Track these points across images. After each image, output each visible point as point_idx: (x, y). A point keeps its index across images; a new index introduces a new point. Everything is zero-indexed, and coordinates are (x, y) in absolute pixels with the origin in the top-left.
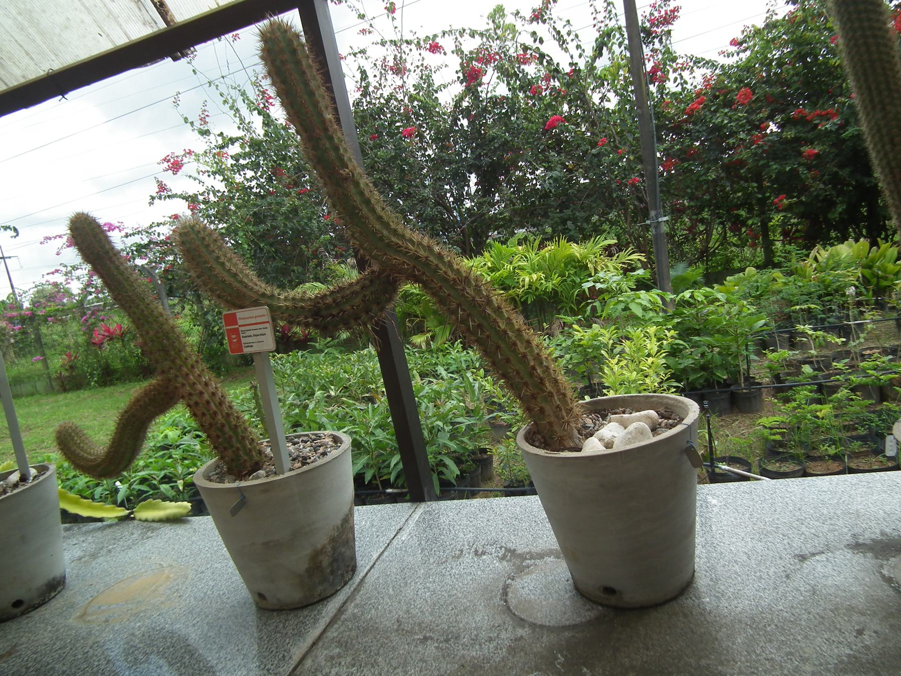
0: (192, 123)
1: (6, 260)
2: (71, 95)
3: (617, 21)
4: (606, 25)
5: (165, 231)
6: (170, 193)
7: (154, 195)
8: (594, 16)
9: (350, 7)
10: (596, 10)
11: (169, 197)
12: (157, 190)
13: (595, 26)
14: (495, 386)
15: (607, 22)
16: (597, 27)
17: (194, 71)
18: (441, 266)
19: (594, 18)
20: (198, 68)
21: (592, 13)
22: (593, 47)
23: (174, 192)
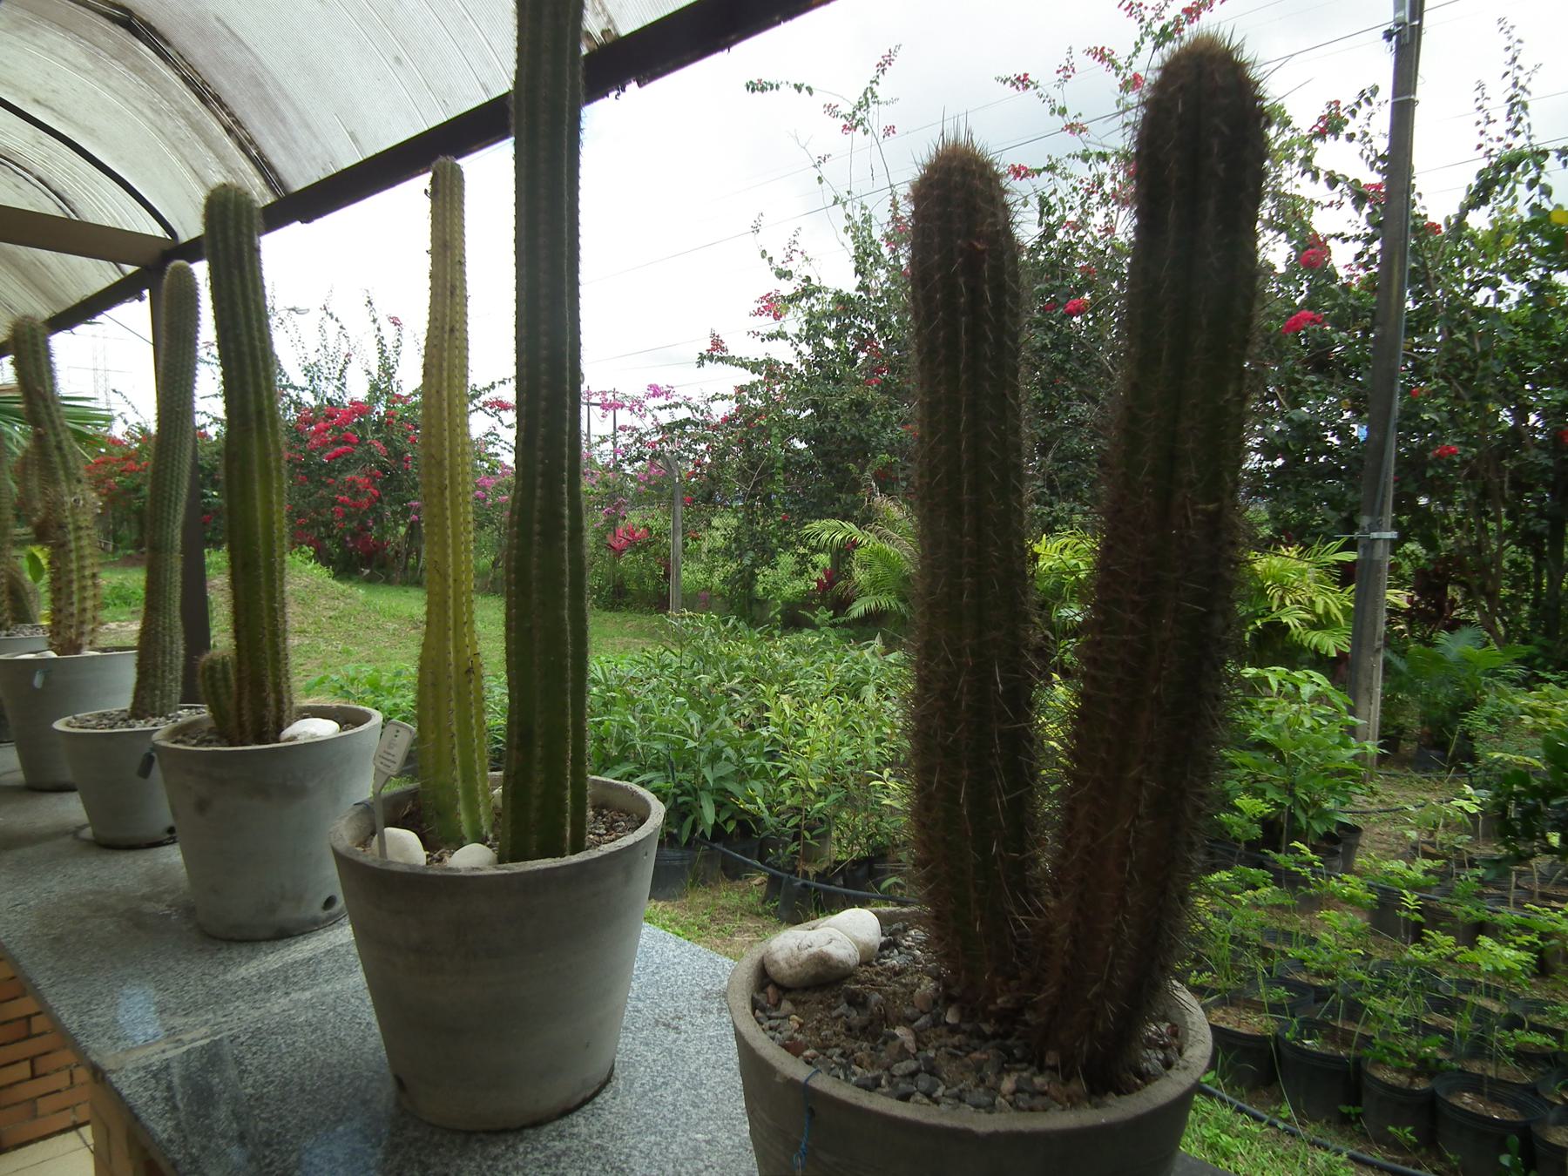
0: (771, 259)
1: (592, 407)
2: (428, 259)
3: (1529, 138)
4: (1509, 146)
5: (721, 410)
6: (724, 354)
7: (705, 353)
8: (1481, 127)
9: (1041, 96)
10: (1488, 117)
11: (721, 359)
12: (710, 347)
13: (1480, 147)
14: (1388, 998)
15: (1510, 139)
16: (1483, 150)
17: (819, 178)
18: (76, 605)
19: (1482, 133)
20: (825, 176)
21: (1478, 123)
22: (1470, 187)
23: (730, 354)
